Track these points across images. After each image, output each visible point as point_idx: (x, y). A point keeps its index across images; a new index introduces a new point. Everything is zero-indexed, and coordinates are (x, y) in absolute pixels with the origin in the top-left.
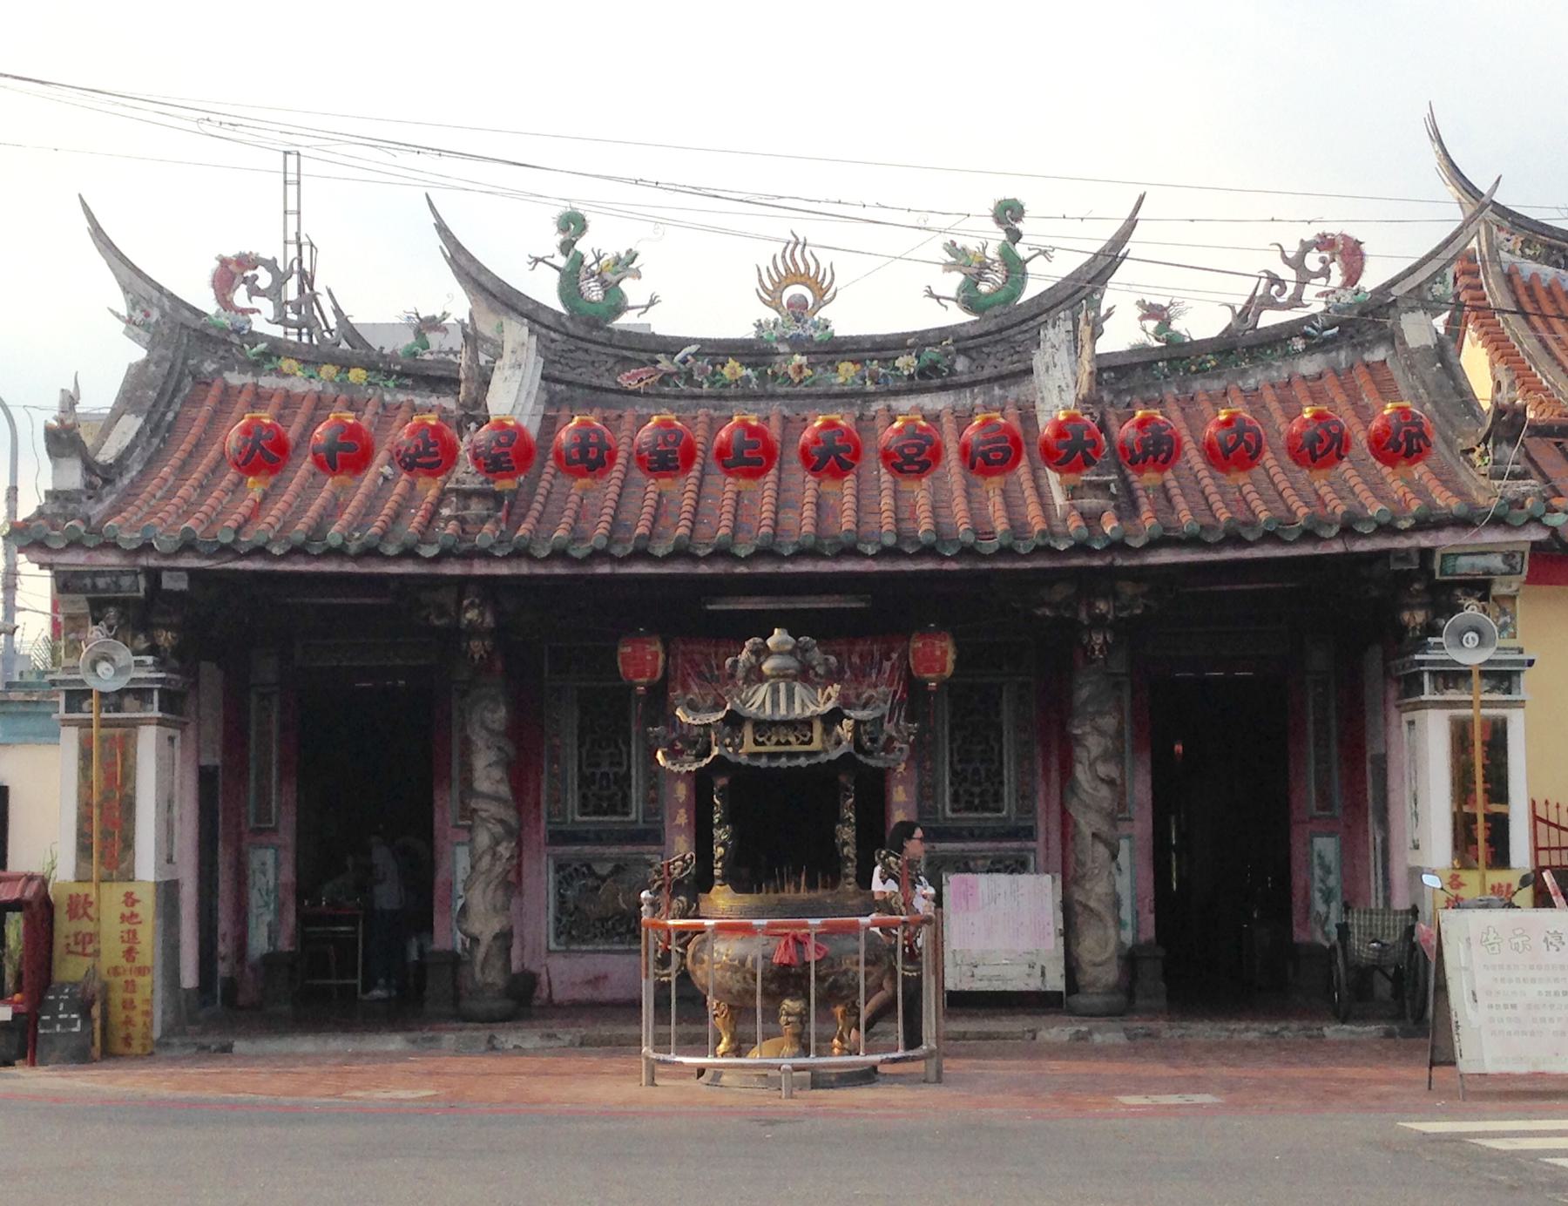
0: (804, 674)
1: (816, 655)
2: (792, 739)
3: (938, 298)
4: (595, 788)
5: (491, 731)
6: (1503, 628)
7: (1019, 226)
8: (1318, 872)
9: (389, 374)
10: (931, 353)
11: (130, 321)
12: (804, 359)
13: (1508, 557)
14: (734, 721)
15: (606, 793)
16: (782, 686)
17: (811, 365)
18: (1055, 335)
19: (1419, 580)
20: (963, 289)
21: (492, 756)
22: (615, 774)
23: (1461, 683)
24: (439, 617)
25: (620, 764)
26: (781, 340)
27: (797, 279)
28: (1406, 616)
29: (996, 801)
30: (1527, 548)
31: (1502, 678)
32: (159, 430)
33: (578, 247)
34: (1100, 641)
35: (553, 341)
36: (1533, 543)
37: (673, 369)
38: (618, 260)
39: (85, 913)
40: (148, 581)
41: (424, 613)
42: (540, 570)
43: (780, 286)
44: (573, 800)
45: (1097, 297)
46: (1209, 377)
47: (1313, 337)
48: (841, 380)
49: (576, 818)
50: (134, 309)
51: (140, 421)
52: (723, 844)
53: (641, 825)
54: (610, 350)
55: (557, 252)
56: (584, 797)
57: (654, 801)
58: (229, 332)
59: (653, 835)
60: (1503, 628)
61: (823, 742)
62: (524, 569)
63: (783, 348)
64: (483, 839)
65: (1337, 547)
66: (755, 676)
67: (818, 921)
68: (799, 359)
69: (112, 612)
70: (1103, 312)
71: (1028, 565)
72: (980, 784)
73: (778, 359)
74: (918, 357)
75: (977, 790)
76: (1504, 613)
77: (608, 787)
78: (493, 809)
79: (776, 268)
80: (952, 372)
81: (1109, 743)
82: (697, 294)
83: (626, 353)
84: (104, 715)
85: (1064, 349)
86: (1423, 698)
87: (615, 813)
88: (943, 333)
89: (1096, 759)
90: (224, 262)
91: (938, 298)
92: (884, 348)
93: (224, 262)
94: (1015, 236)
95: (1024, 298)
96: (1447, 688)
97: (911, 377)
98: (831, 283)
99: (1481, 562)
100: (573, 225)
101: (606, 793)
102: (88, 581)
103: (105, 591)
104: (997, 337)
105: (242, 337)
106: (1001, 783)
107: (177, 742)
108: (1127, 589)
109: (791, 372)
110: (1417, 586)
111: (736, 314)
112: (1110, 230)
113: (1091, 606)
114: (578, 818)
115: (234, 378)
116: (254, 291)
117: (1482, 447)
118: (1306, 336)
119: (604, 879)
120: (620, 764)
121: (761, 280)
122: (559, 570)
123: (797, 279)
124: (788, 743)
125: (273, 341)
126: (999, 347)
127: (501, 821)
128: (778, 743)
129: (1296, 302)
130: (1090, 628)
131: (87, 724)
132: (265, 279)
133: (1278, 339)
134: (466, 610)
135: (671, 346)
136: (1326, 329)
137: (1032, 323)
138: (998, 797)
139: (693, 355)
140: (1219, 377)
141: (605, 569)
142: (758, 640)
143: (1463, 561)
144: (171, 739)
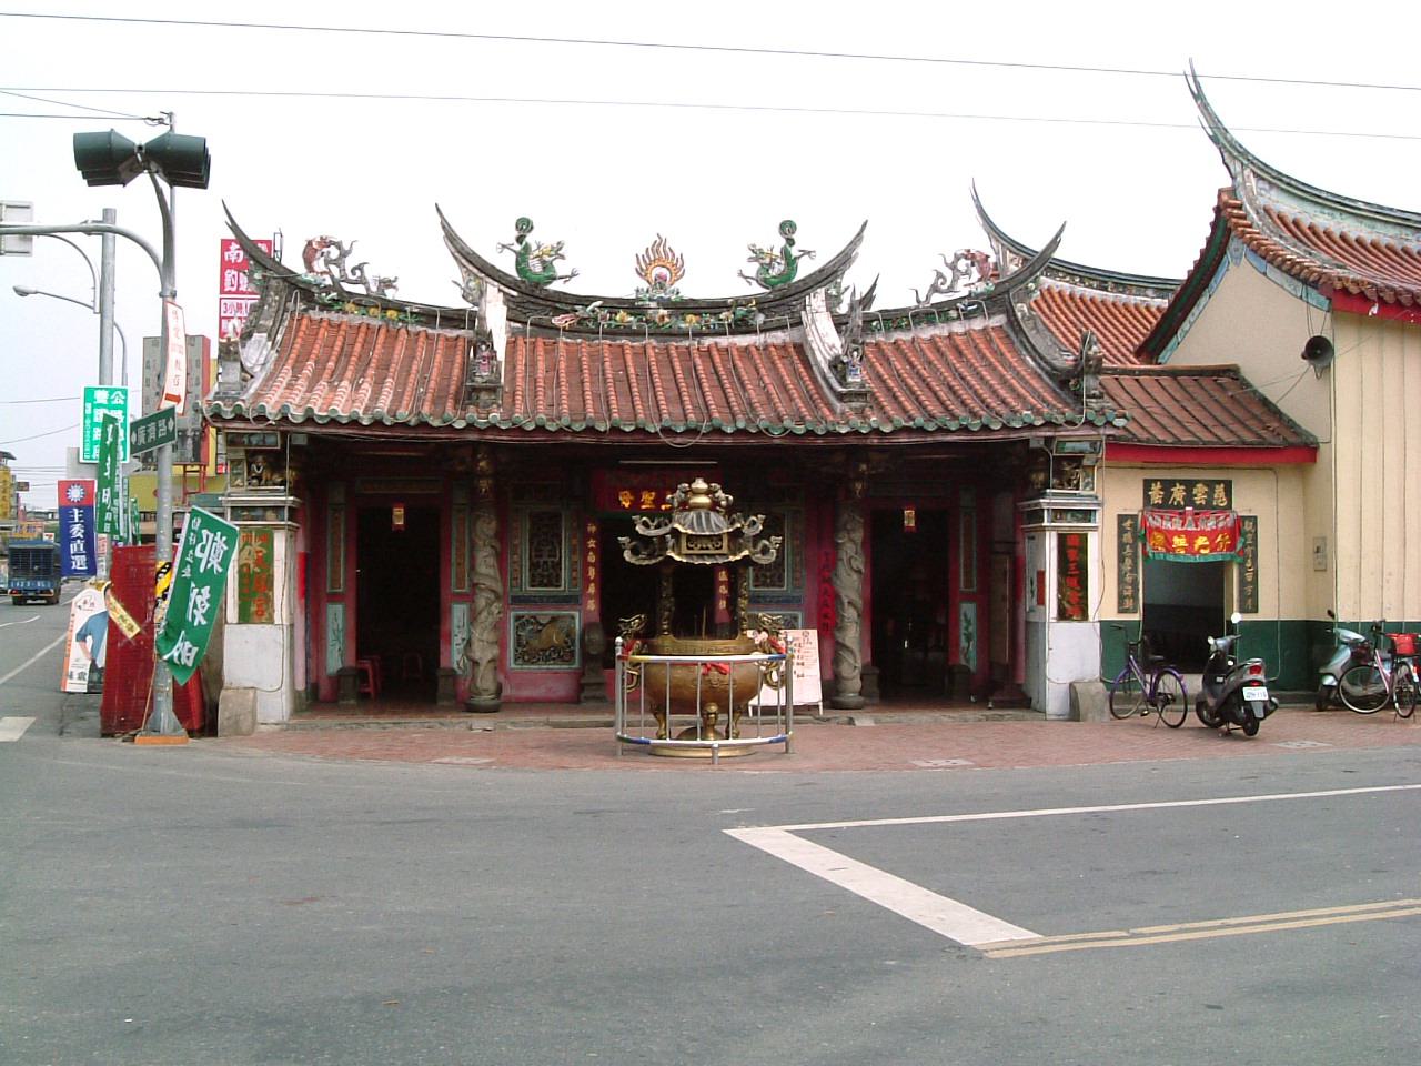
2: (710, 546)
3: (746, 278)
4: (540, 570)
6: (1087, 484)
7: (794, 236)
8: (964, 624)
10: (741, 311)
12: (665, 312)
13: (1093, 444)
14: (675, 533)
15: (546, 573)
17: (669, 316)
18: (817, 301)
22: (552, 562)
25: (555, 556)
27: (659, 259)
28: (1034, 476)
31: (1087, 515)
34: (860, 487)
40: (281, 436)
45: (839, 280)
49: (528, 589)
55: (515, 243)
63: (653, 305)
66: (685, 506)
68: (663, 312)
70: (843, 288)
72: (547, 570)
73: (650, 311)
75: (768, 574)
76: (1087, 476)
79: (649, 257)
82: (599, 270)
87: (552, 585)
92: (716, 307)
94: (791, 242)
95: (795, 280)
99: (1078, 446)
100: (524, 226)
101: (546, 573)
102: (246, 439)
103: (257, 445)
108: (875, 456)
109: (657, 320)
111: (625, 285)
114: (529, 588)
119: (544, 625)
120: (555, 556)
123: (659, 259)
124: (707, 548)
127: (493, 591)
128: (702, 548)
129: (951, 289)
134: (479, 461)
135: (586, 301)
139: (600, 307)
143: (1068, 445)
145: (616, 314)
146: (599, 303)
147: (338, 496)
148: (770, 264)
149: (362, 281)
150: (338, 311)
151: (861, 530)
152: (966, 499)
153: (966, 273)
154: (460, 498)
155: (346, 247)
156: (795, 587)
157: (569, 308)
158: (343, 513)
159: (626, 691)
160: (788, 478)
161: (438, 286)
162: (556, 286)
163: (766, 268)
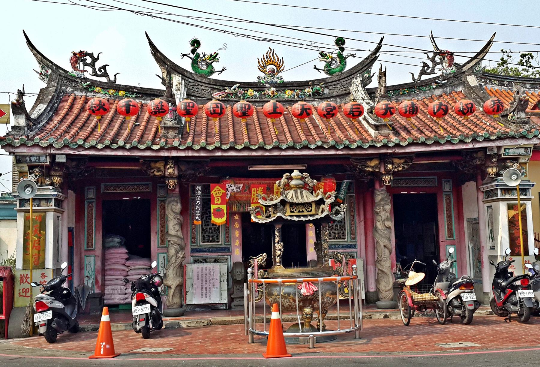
0: (305, 186)
1: (309, 180)
2: (304, 210)
3: (318, 69)
5: (176, 213)
9: (133, 93)
11: (41, 74)
12: (275, 89)
16: (299, 191)
17: (277, 91)
19: (495, 158)
20: (325, 67)
21: (176, 222)
22: (215, 228)
23: (510, 192)
24: (158, 172)
26: (267, 83)
27: (271, 63)
28: (490, 170)
29: (343, 236)
30: (532, 146)
32: (52, 109)
33: (198, 51)
35: (190, 82)
36: (535, 145)
37: (231, 92)
38: (211, 55)
39: (26, 281)
40: (50, 158)
41: (153, 171)
42: (196, 154)
43: (265, 67)
44: (200, 237)
46: (406, 96)
47: (439, 83)
48: (287, 96)
50: (42, 69)
51: (45, 106)
52: (280, 250)
53: (223, 246)
54: (210, 86)
55: (190, 52)
56: (204, 236)
57: (228, 237)
58: (76, 78)
59: (227, 249)
60: (523, 174)
61: (316, 211)
62: (190, 154)
63: (268, 85)
64: (172, 251)
65: (471, 146)
66: (287, 187)
67: (322, 279)
68: (273, 89)
69: (37, 170)
71: (366, 152)
72: (212, 233)
73: (266, 89)
74: (312, 89)
75: (336, 232)
77: (212, 233)
78: (176, 239)
79: (264, 59)
80: (324, 94)
81: (388, 215)
82: (239, 66)
83: (215, 87)
84: (34, 208)
85: (360, 86)
86: (498, 197)
87: (214, 241)
88: (320, 81)
89: (384, 220)
90: (75, 54)
91: (318, 69)
93: (75, 54)
96: (506, 194)
97: (310, 95)
98: (283, 64)
100: (196, 43)
101: (211, 235)
102: (28, 159)
103: (34, 162)
104: (338, 82)
105: (81, 79)
106: (345, 229)
107: (60, 218)
108: (396, 161)
109: (270, 93)
110: (494, 160)
111: (252, 75)
112: (373, 47)
113: (385, 167)
115: (78, 93)
116: (86, 64)
117: (512, 114)
118: (436, 83)
121: (259, 63)
122: (203, 154)
123: (271, 63)
124: (303, 212)
125: (93, 81)
126: (338, 86)
127: (178, 245)
128: (299, 212)
129: (432, 72)
130: (385, 174)
131: (27, 211)
132: (89, 60)
133: (427, 83)
134: (168, 169)
135: (230, 84)
136: (442, 81)
137: (349, 78)
138: (344, 234)
139: (238, 87)
140: (409, 96)
141: (219, 154)
142: (289, 174)
144: (58, 217)
145: (247, 91)
146: (238, 85)
147: (91, 194)
148: (331, 62)
149: (105, 75)
150: (91, 92)
151: (390, 204)
152: (447, 187)
153: (441, 63)
154: (161, 193)
155: (96, 56)
156: (351, 238)
157: (221, 88)
158: (94, 204)
159: (254, 302)
160: (347, 173)
161: (151, 77)
162: (215, 76)
163: (329, 64)
